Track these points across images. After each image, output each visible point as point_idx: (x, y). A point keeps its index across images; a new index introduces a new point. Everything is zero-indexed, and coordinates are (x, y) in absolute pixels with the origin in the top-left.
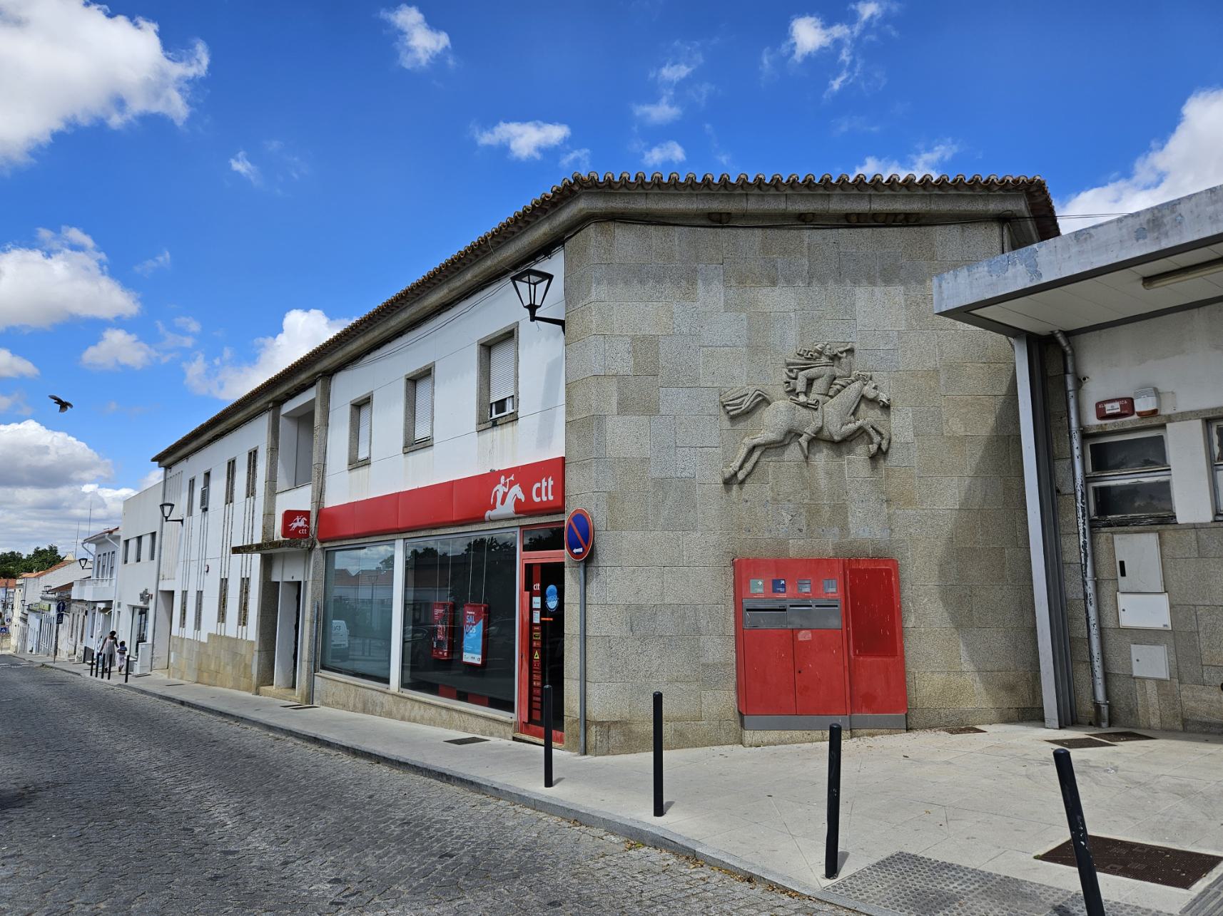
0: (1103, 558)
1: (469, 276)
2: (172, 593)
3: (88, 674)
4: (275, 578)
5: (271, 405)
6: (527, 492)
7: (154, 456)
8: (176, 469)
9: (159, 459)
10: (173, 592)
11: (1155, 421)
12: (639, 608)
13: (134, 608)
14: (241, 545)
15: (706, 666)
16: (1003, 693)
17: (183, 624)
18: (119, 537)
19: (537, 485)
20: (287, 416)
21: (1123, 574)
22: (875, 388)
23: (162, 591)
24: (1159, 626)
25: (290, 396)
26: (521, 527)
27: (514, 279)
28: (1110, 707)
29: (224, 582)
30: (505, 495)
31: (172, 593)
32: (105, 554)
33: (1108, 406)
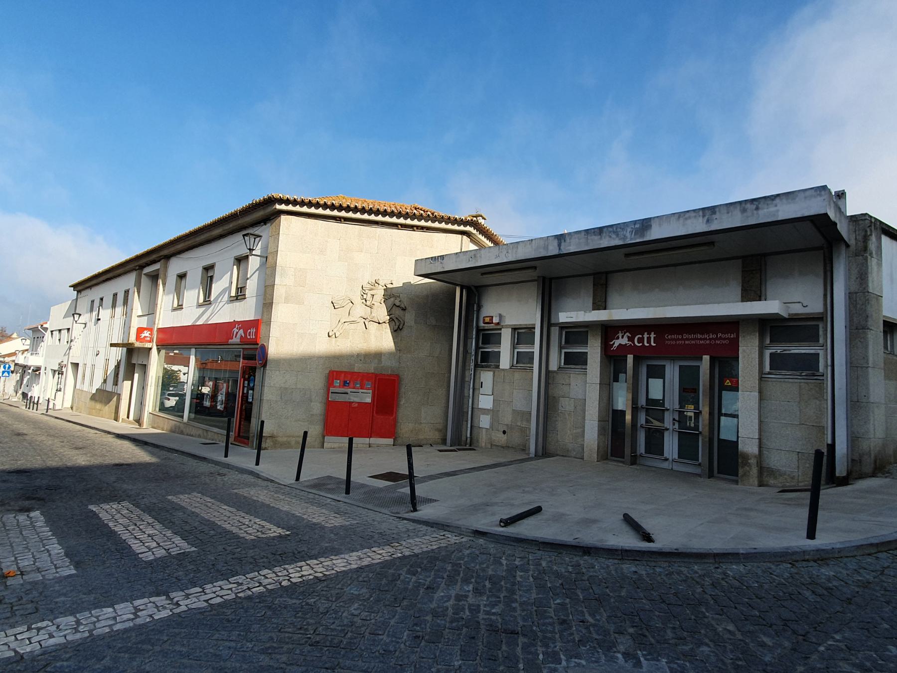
0: (477, 381)
1: (231, 225)
2: (77, 364)
3: (24, 408)
4: (134, 362)
5: (137, 268)
6: (245, 332)
7: (71, 284)
8: (84, 293)
9: (75, 286)
10: (78, 364)
11: (499, 327)
12: (286, 389)
13: (55, 371)
14: (116, 342)
15: (312, 415)
16: (437, 433)
17: (83, 382)
18: (47, 329)
19: (249, 330)
20: (146, 275)
21: (482, 387)
22: (400, 301)
23: (71, 363)
24: (489, 408)
25: (148, 264)
26: (243, 348)
27: (244, 236)
28: (471, 438)
29: (107, 360)
30: (237, 333)
31: (77, 364)
32: (38, 338)
33: (486, 319)
